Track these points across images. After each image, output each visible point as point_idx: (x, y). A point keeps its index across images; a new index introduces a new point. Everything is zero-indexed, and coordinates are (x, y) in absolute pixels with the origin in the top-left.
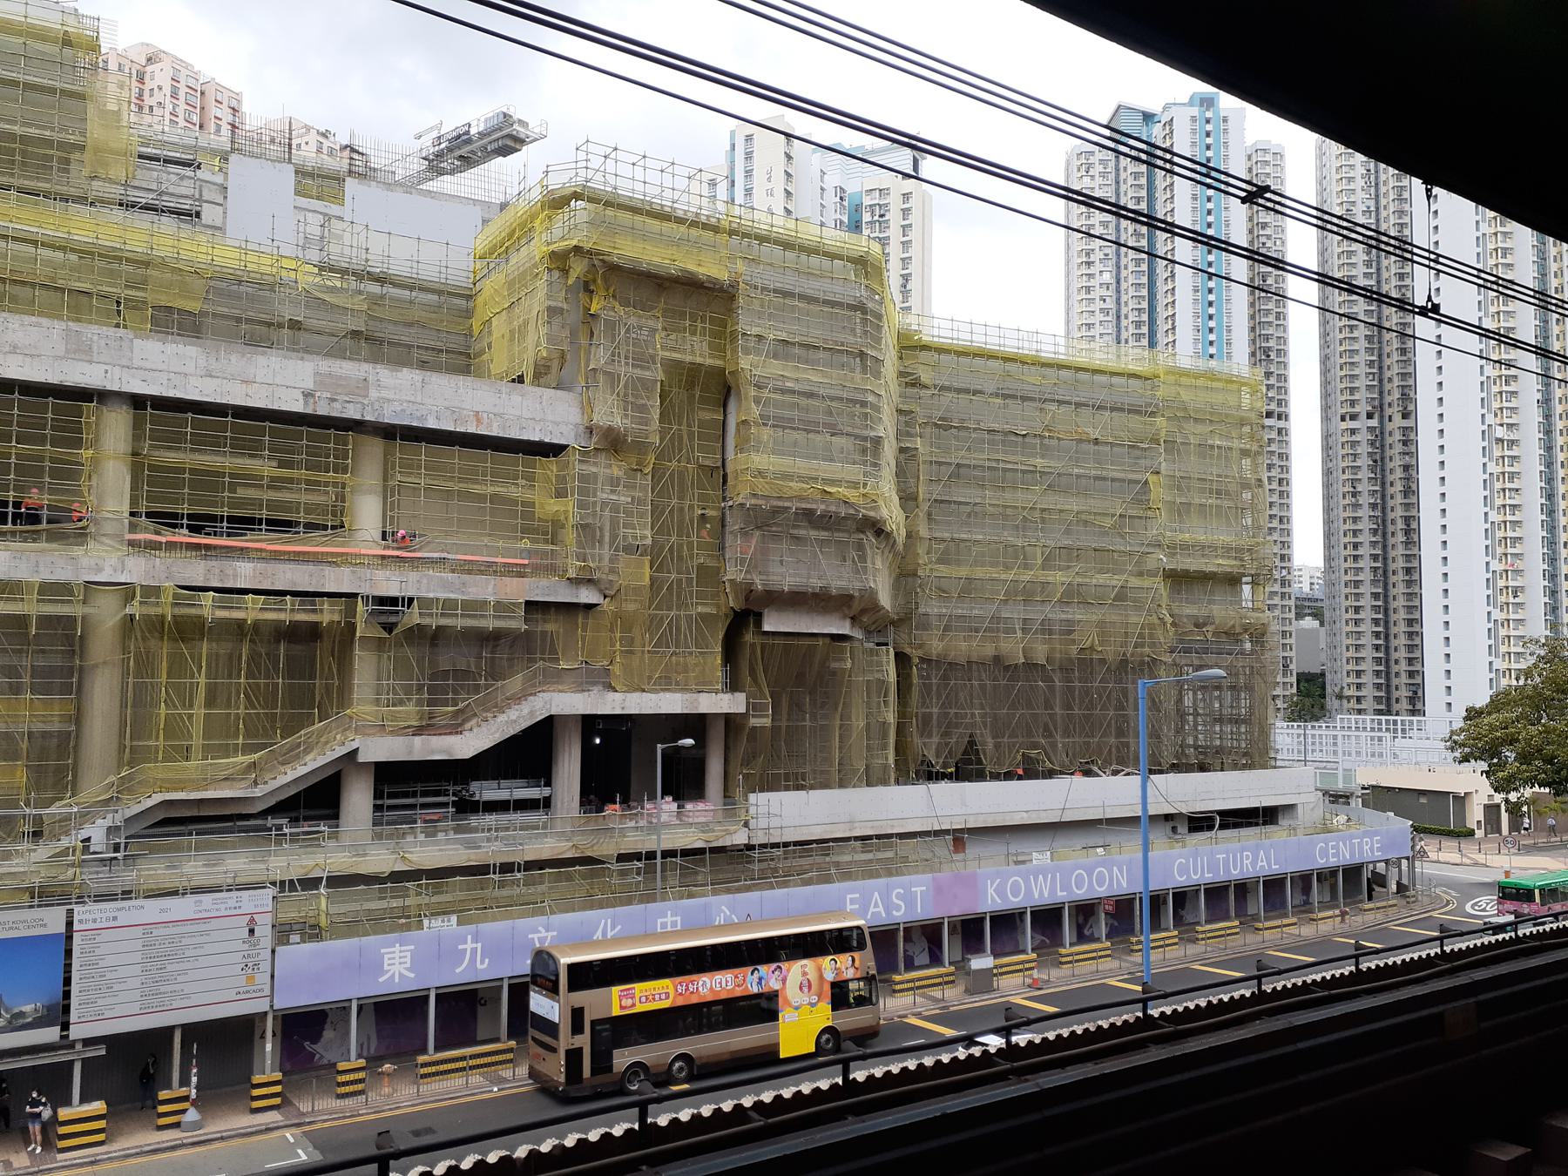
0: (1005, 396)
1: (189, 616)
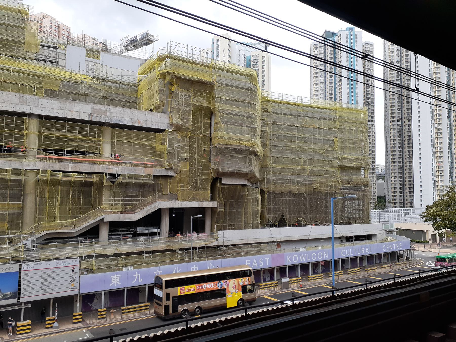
0: (292, 115)
1: (55, 179)
